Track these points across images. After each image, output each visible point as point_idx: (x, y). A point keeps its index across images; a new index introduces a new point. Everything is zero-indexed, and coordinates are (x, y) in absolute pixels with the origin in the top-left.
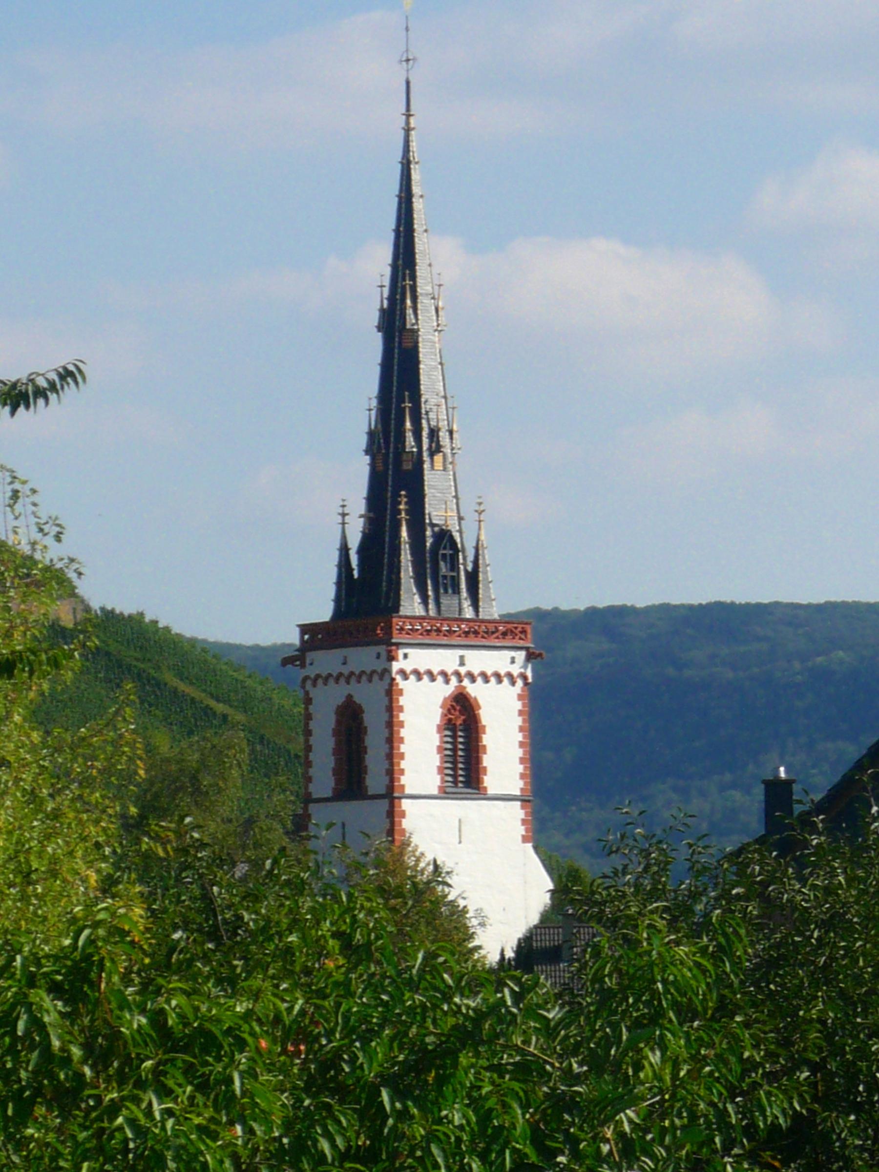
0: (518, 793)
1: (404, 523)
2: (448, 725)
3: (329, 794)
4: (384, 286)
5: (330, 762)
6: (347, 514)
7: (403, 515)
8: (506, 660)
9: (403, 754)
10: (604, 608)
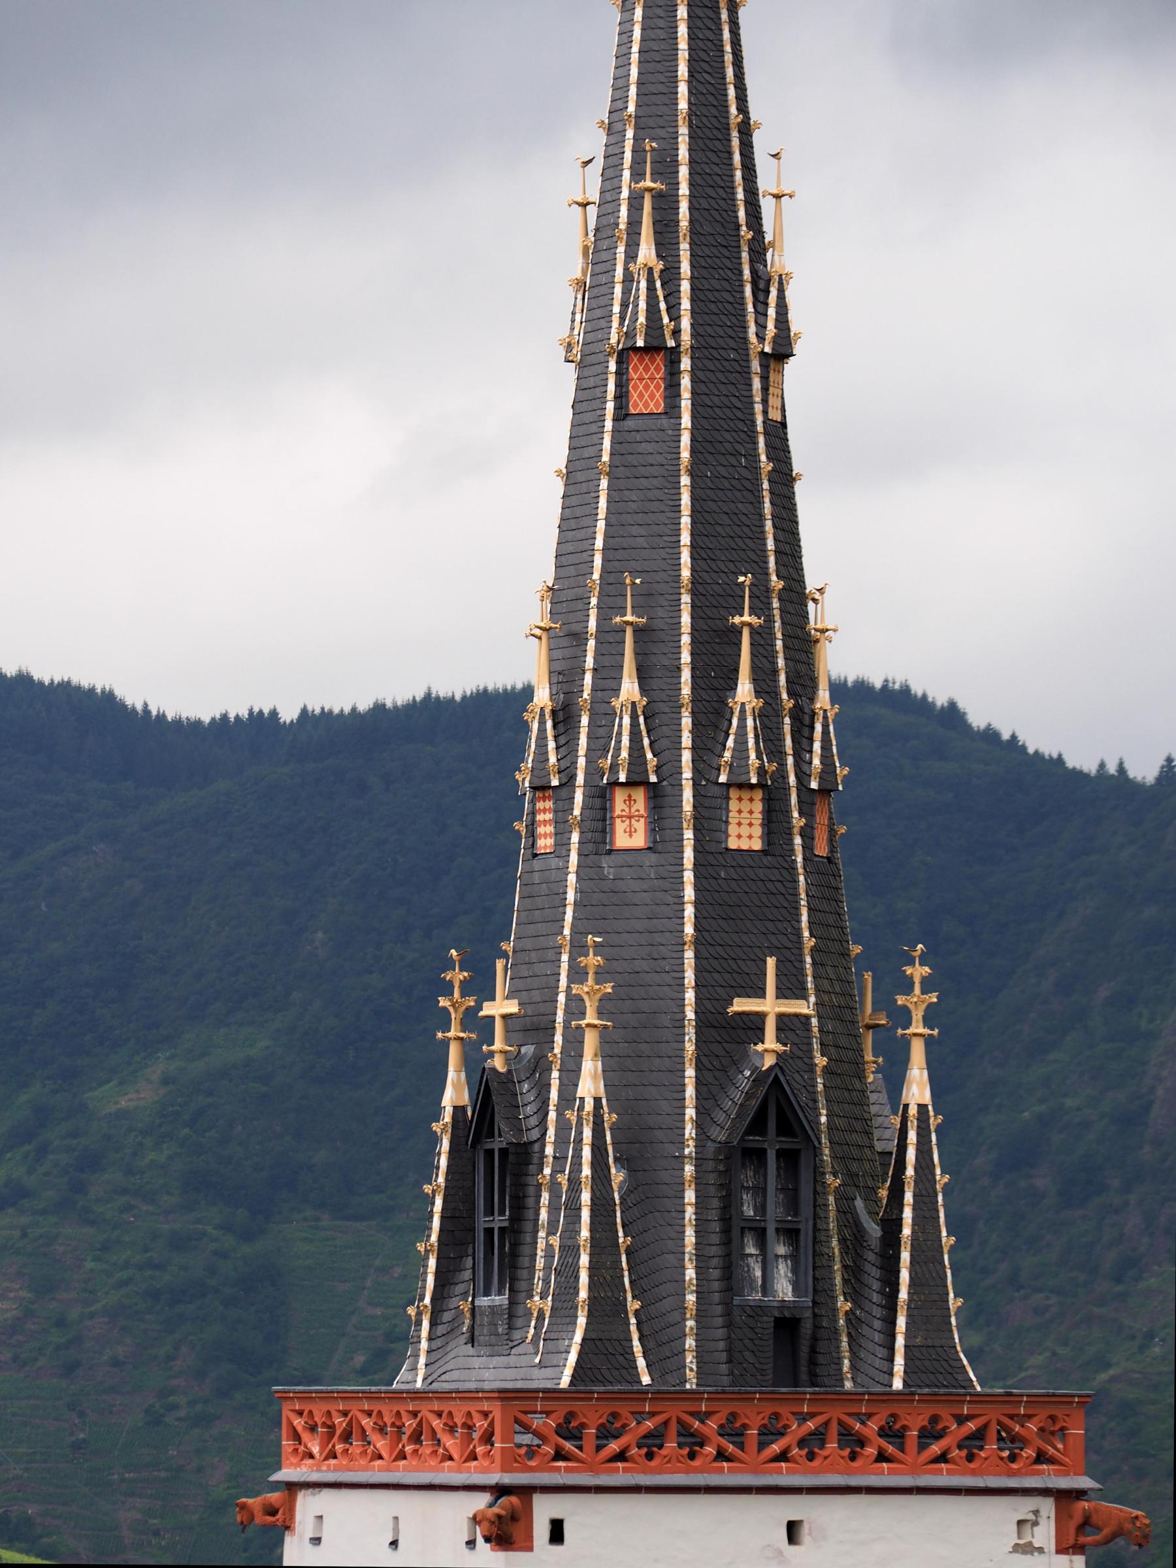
1: (918, 1052)
7: (917, 1027)
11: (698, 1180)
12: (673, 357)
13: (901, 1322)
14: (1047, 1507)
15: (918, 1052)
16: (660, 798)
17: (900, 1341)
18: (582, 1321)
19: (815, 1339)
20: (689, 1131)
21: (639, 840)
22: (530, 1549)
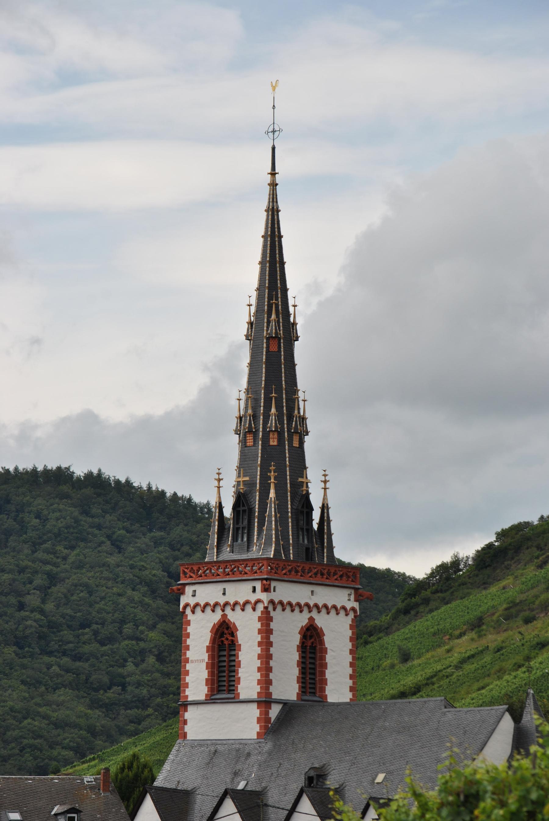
0: (255, 696)
1: (272, 486)
2: (303, 648)
3: (202, 697)
4: (251, 305)
5: (242, 673)
6: (222, 479)
7: (272, 480)
8: (342, 597)
9: (188, 671)
10: (370, 567)
11: (292, 517)
12: (279, 339)
13: (325, 550)
14: (353, 592)
15: (272, 486)
16: (280, 434)
17: (325, 554)
18: (274, 545)
19: (312, 552)
20: (289, 506)
21: (275, 443)
22: (270, 592)
